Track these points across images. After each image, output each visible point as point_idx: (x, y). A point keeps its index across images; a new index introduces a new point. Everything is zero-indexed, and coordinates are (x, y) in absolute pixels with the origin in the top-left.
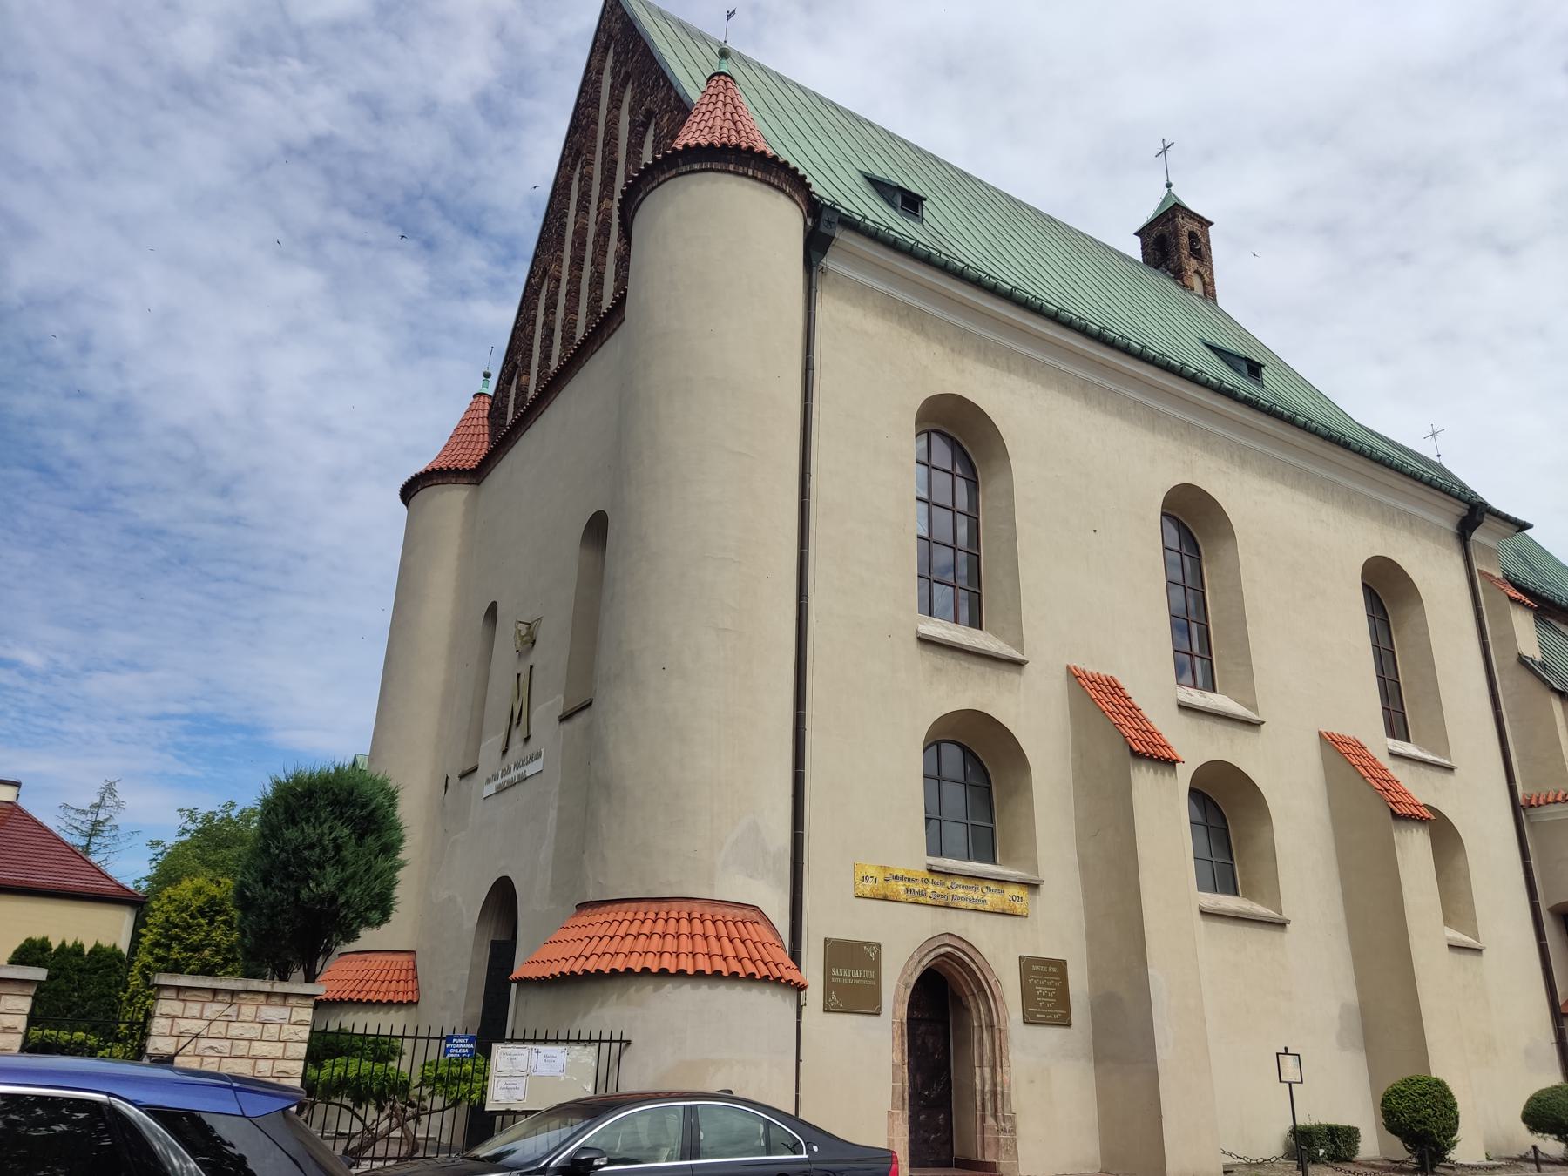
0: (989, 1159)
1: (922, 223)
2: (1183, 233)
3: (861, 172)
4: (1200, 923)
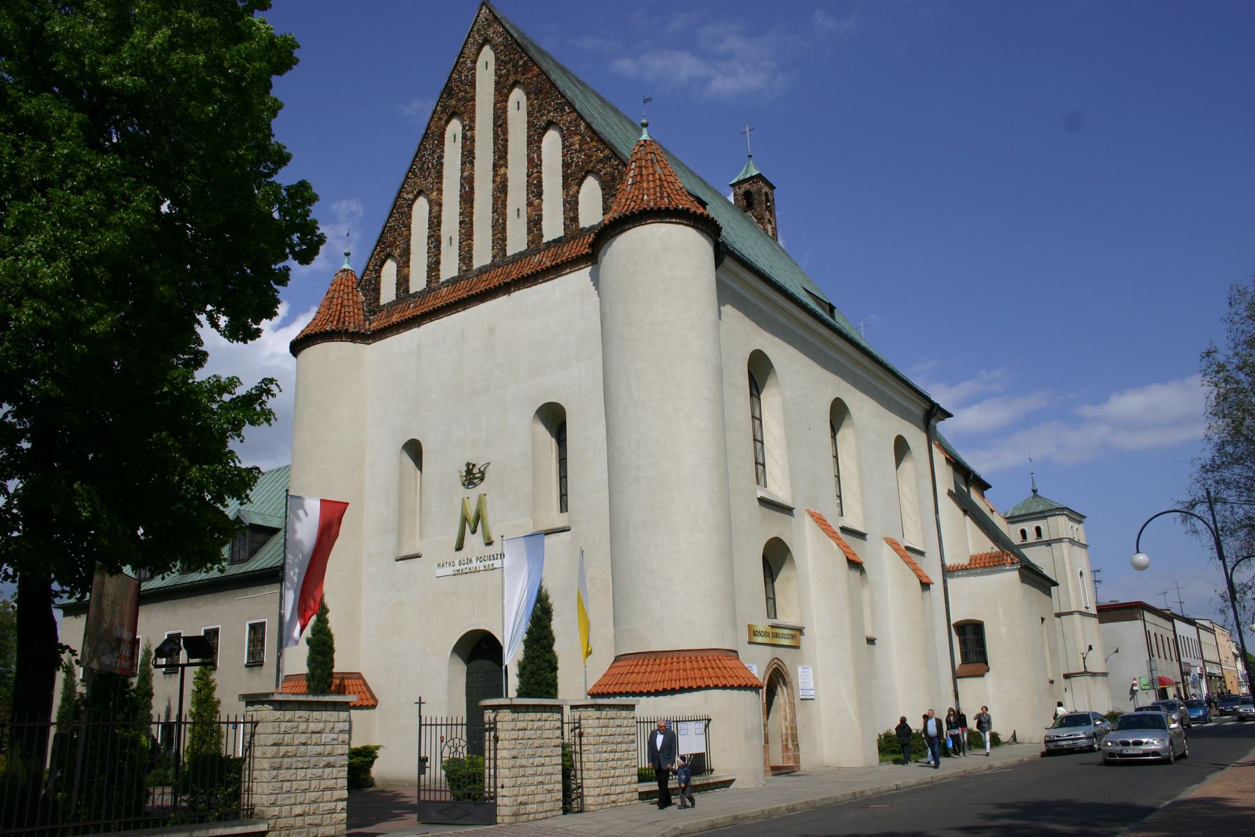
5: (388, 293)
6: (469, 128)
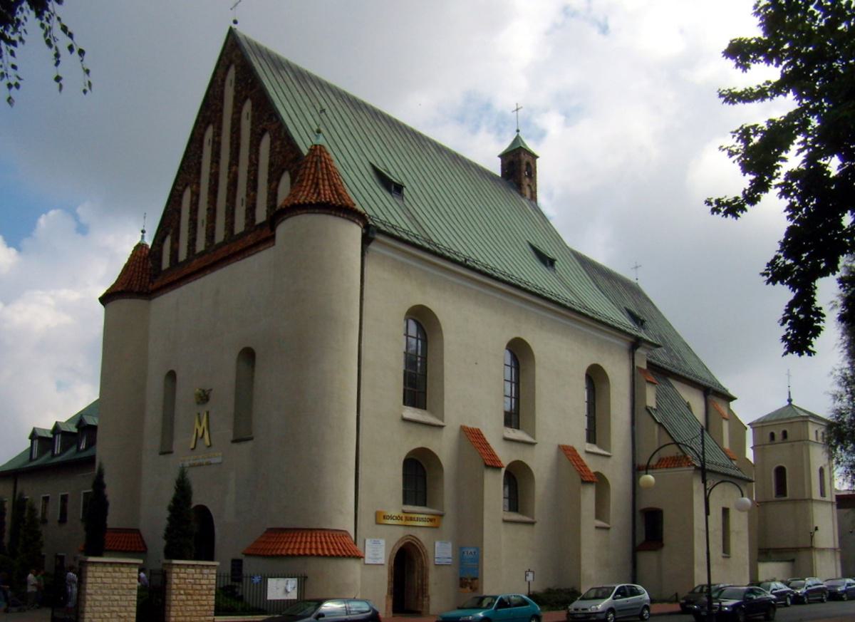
0: (419, 609)
1: (403, 199)
3: (371, 163)
4: (502, 526)
5: (166, 264)
6: (218, 133)
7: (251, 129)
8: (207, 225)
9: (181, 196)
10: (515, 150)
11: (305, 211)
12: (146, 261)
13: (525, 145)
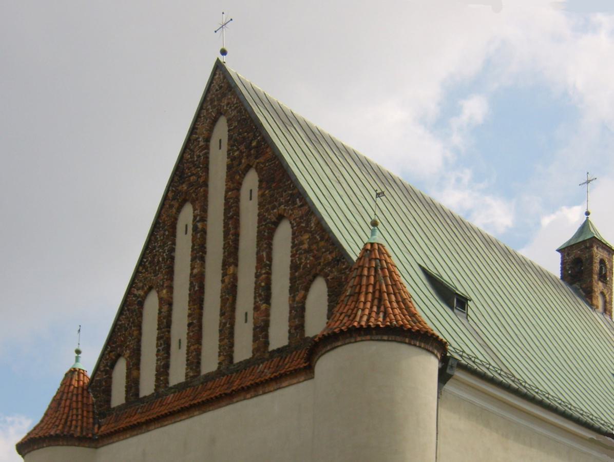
2: (596, 261)
5: (118, 397)
6: (201, 217)
7: (259, 215)
8: (188, 347)
9: (141, 304)
10: (584, 242)
11: (368, 337)
12: (85, 392)
13: (598, 234)
